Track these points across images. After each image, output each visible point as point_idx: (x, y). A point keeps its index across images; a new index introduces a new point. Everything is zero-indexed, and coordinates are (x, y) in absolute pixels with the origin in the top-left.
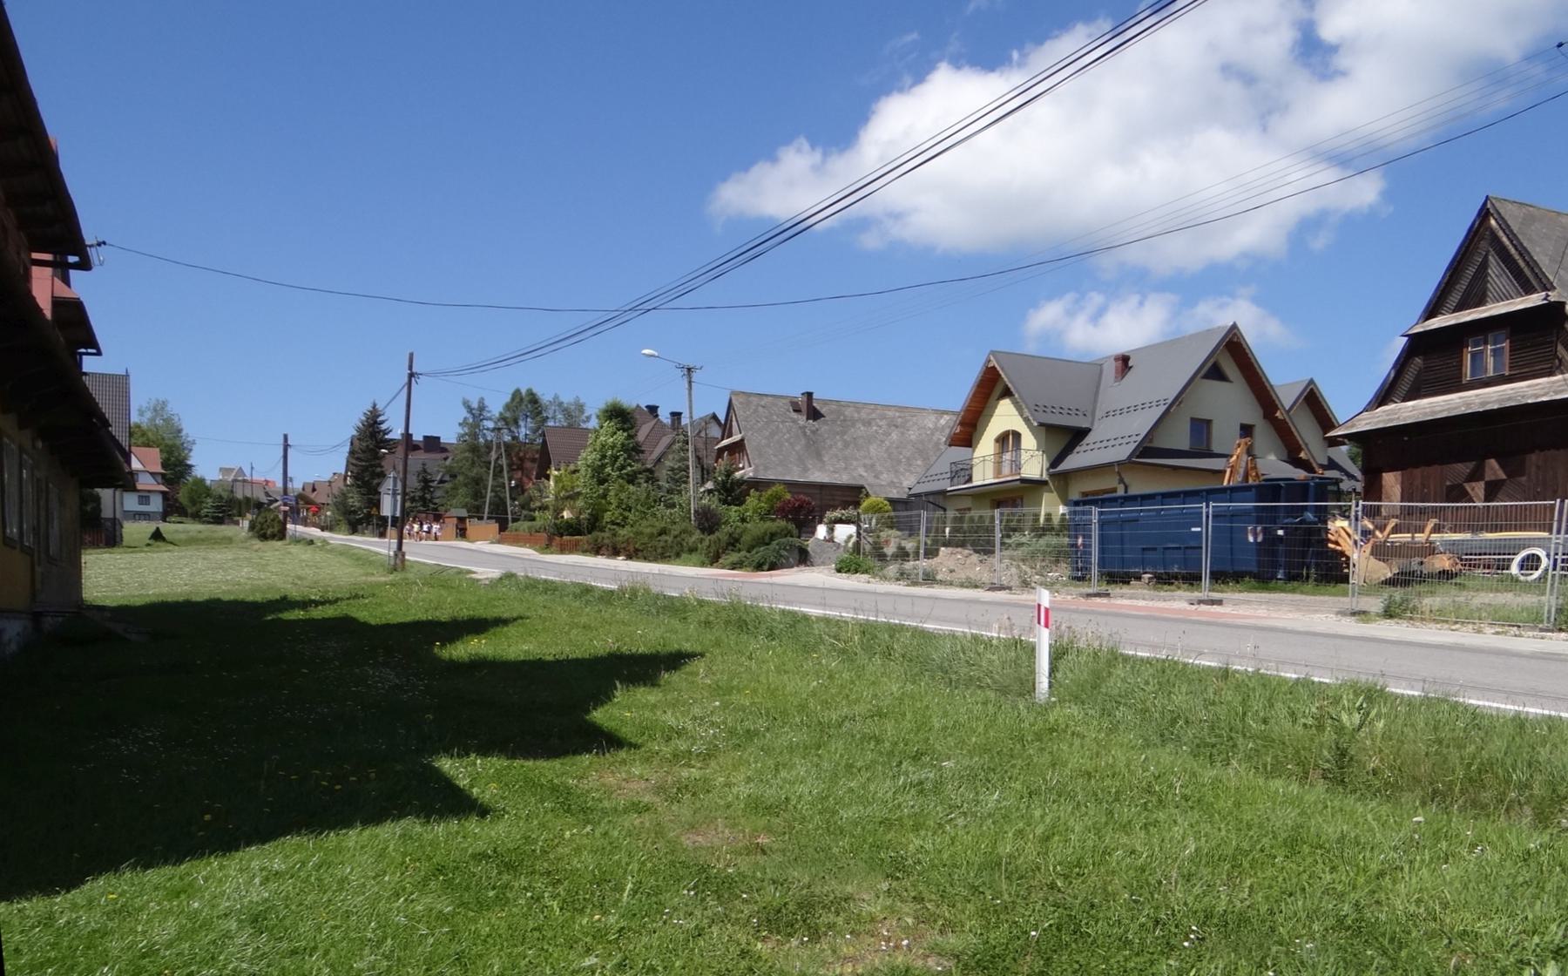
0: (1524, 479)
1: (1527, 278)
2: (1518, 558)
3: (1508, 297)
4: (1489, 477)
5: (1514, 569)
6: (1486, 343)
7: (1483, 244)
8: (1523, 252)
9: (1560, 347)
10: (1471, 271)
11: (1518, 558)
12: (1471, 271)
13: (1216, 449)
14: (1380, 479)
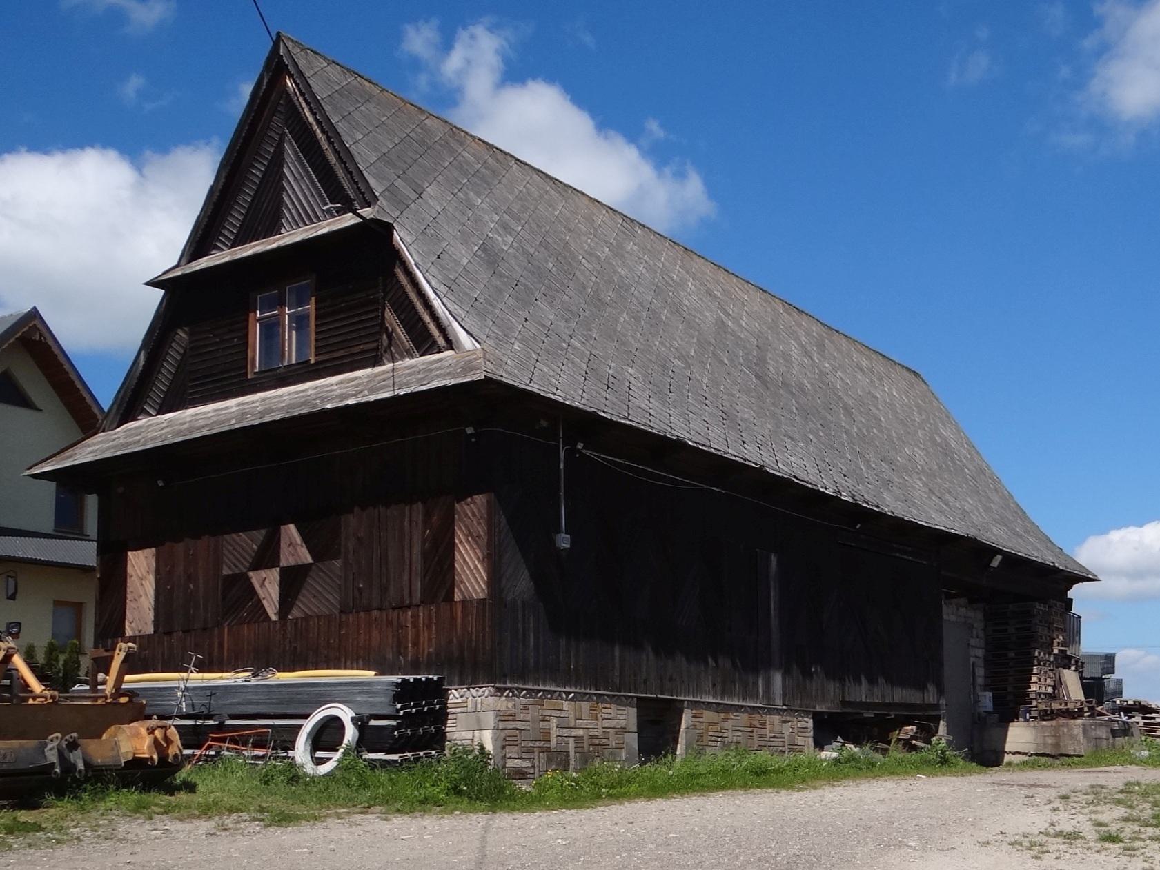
0: (338, 563)
1: (340, 185)
2: (302, 741)
3: (313, 218)
4: (286, 560)
5: (301, 752)
6: (282, 304)
7: (277, 121)
8: (345, 156)
9: (388, 314)
10: (258, 171)
11: (308, 725)
12: (258, 171)
13: (51, 486)
14: (279, 530)
